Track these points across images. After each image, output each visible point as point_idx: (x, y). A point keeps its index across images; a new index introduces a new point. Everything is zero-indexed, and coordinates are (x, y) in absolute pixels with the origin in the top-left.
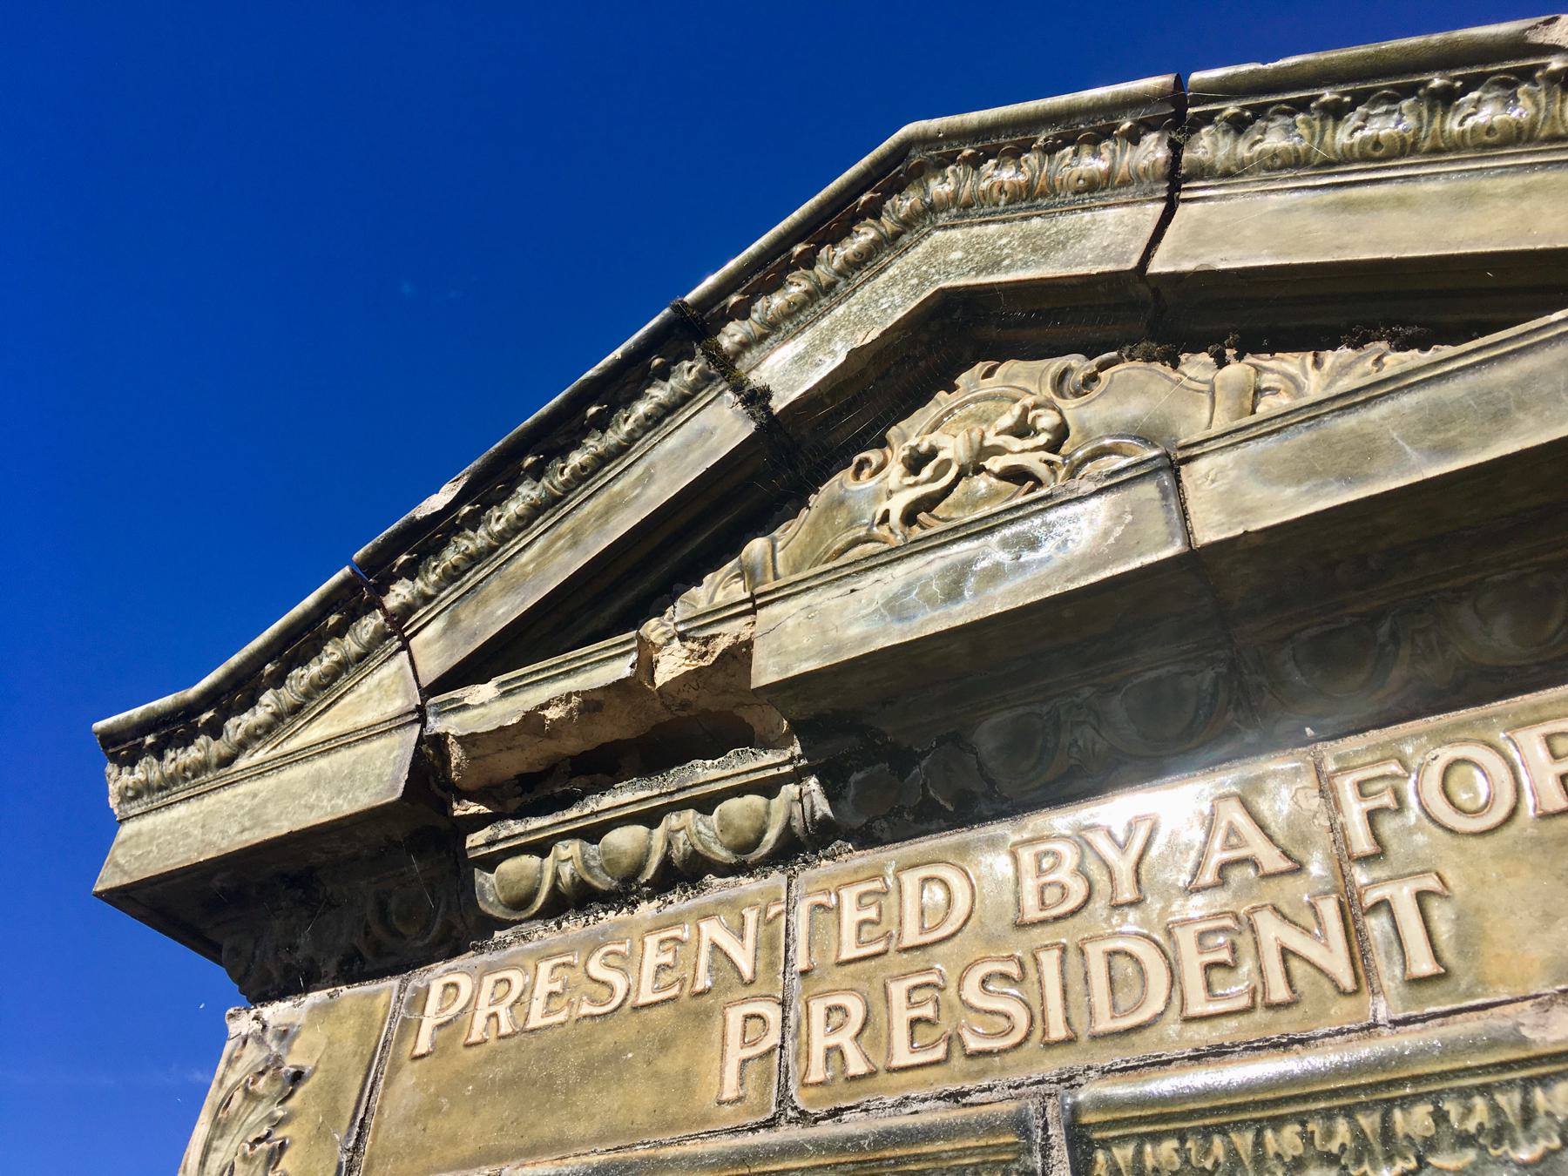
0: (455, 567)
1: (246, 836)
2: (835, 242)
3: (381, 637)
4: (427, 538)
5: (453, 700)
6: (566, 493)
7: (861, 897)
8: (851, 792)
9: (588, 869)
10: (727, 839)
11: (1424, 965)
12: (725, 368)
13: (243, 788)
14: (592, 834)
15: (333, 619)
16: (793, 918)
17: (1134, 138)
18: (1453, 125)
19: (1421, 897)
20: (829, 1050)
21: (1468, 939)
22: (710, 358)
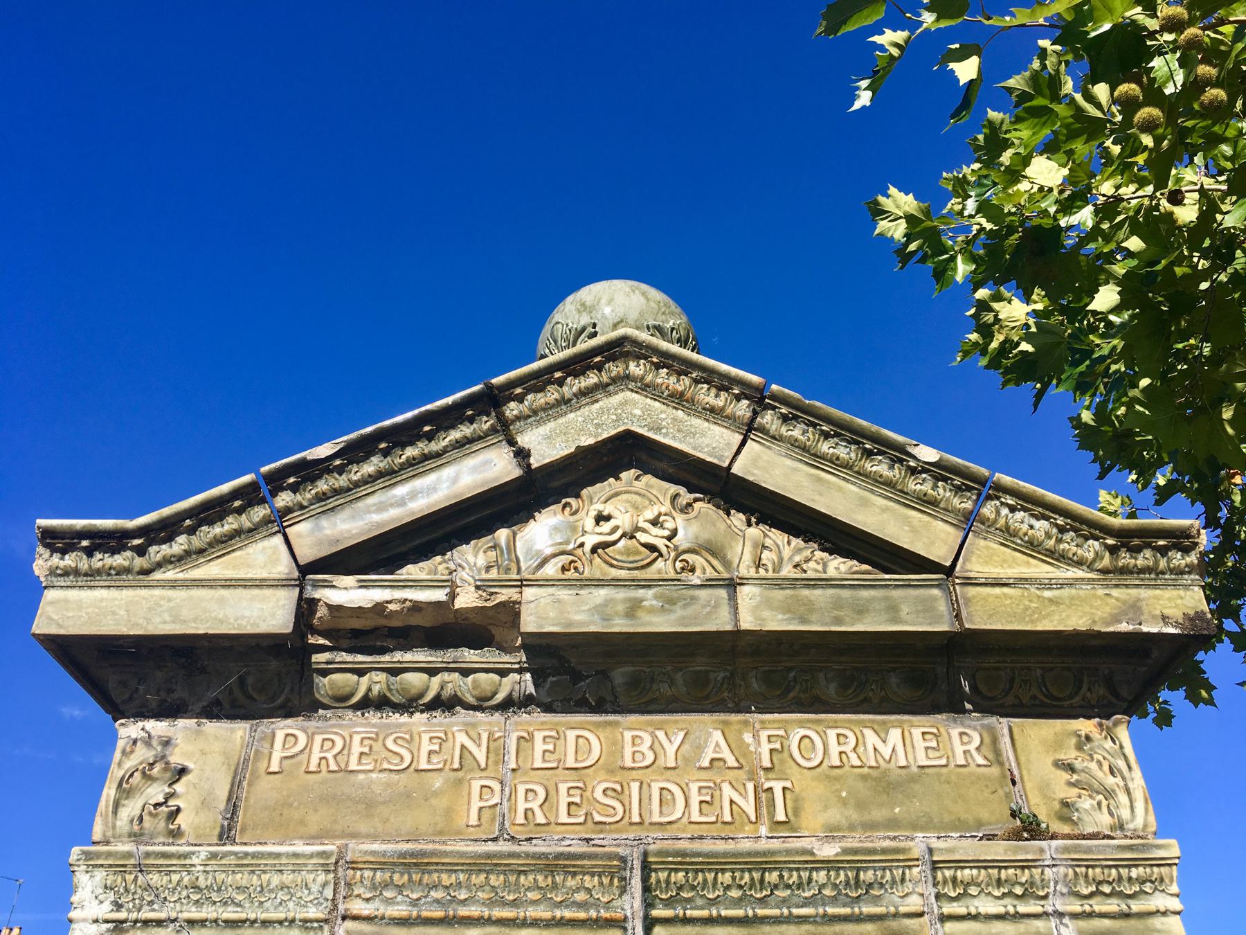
0: (324, 494)
1: (161, 626)
3: (266, 521)
4: (309, 472)
5: (325, 581)
6: (401, 469)
7: (545, 738)
8: (548, 685)
9: (390, 690)
10: (475, 693)
11: (781, 817)
12: (505, 431)
13: (157, 592)
14: (394, 672)
15: (237, 503)
16: (508, 741)
17: (738, 398)
19: (784, 789)
20: (526, 810)
21: (797, 812)
22: (499, 420)
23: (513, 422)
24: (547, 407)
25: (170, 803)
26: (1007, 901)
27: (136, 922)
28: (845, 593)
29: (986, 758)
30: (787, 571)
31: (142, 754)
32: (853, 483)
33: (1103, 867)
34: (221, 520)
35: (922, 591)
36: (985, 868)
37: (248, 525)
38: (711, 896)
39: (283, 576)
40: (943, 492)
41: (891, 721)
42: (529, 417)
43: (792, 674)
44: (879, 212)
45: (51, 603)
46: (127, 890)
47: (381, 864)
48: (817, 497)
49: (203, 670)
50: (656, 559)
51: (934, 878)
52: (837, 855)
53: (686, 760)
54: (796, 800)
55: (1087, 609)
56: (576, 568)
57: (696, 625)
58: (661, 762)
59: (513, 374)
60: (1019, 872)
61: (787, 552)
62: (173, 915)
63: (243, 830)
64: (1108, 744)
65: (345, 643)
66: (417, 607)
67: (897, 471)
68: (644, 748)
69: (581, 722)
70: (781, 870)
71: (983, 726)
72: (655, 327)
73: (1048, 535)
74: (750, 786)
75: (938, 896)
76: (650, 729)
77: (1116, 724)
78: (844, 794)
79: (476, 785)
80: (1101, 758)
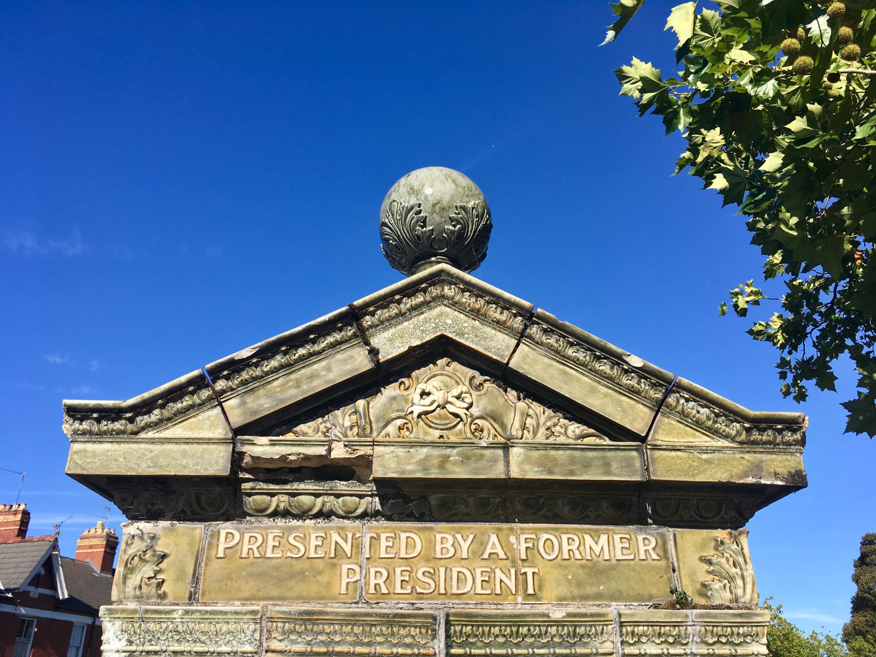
2: (409, 297)
3: (210, 399)
7: (387, 538)
9: (290, 506)
10: (344, 509)
11: (530, 591)
12: (363, 337)
13: (143, 446)
15: (191, 388)
18: (597, 365)
19: (534, 573)
20: (376, 584)
21: (540, 588)
22: (359, 329)
23: (368, 329)
24: (390, 319)
25: (158, 576)
26: (663, 646)
27: (142, 652)
28: (578, 454)
29: (658, 555)
30: (541, 438)
31: (138, 546)
32: (586, 376)
33: (723, 627)
34: (181, 398)
35: (626, 453)
36: (652, 626)
37: (198, 401)
38: (487, 641)
39: (223, 437)
40: (644, 386)
41: (602, 530)
42: (378, 325)
43: (542, 500)
44: (623, 77)
45: (76, 452)
46: (135, 633)
47: (288, 618)
48: (563, 386)
49: (174, 492)
50: (458, 423)
51: (621, 632)
52: (563, 617)
53: (474, 553)
54: (540, 580)
55: (728, 467)
56: (407, 428)
57: (483, 474)
58: (458, 555)
59: (367, 298)
60: (672, 629)
61: (542, 419)
62: (164, 648)
63: (203, 594)
64: (734, 547)
65: (261, 476)
66: (307, 458)
67: (615, 371)
68: (449, 545)
69: (410, 527)
70: (529, 626)
71: (658, 534)
72: (461, 207)
73: (708, 418)
74: (513, 571)
75: (622, 643)
76: (452, 533)
77: (740, 534)
78: (570, 577)
79: (345, 568)
80: (728, 556)
